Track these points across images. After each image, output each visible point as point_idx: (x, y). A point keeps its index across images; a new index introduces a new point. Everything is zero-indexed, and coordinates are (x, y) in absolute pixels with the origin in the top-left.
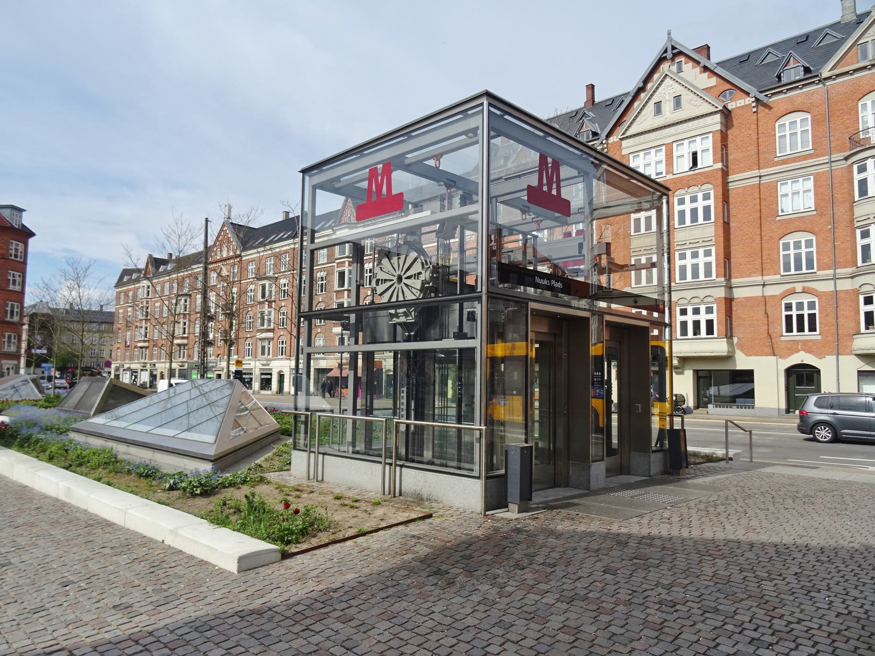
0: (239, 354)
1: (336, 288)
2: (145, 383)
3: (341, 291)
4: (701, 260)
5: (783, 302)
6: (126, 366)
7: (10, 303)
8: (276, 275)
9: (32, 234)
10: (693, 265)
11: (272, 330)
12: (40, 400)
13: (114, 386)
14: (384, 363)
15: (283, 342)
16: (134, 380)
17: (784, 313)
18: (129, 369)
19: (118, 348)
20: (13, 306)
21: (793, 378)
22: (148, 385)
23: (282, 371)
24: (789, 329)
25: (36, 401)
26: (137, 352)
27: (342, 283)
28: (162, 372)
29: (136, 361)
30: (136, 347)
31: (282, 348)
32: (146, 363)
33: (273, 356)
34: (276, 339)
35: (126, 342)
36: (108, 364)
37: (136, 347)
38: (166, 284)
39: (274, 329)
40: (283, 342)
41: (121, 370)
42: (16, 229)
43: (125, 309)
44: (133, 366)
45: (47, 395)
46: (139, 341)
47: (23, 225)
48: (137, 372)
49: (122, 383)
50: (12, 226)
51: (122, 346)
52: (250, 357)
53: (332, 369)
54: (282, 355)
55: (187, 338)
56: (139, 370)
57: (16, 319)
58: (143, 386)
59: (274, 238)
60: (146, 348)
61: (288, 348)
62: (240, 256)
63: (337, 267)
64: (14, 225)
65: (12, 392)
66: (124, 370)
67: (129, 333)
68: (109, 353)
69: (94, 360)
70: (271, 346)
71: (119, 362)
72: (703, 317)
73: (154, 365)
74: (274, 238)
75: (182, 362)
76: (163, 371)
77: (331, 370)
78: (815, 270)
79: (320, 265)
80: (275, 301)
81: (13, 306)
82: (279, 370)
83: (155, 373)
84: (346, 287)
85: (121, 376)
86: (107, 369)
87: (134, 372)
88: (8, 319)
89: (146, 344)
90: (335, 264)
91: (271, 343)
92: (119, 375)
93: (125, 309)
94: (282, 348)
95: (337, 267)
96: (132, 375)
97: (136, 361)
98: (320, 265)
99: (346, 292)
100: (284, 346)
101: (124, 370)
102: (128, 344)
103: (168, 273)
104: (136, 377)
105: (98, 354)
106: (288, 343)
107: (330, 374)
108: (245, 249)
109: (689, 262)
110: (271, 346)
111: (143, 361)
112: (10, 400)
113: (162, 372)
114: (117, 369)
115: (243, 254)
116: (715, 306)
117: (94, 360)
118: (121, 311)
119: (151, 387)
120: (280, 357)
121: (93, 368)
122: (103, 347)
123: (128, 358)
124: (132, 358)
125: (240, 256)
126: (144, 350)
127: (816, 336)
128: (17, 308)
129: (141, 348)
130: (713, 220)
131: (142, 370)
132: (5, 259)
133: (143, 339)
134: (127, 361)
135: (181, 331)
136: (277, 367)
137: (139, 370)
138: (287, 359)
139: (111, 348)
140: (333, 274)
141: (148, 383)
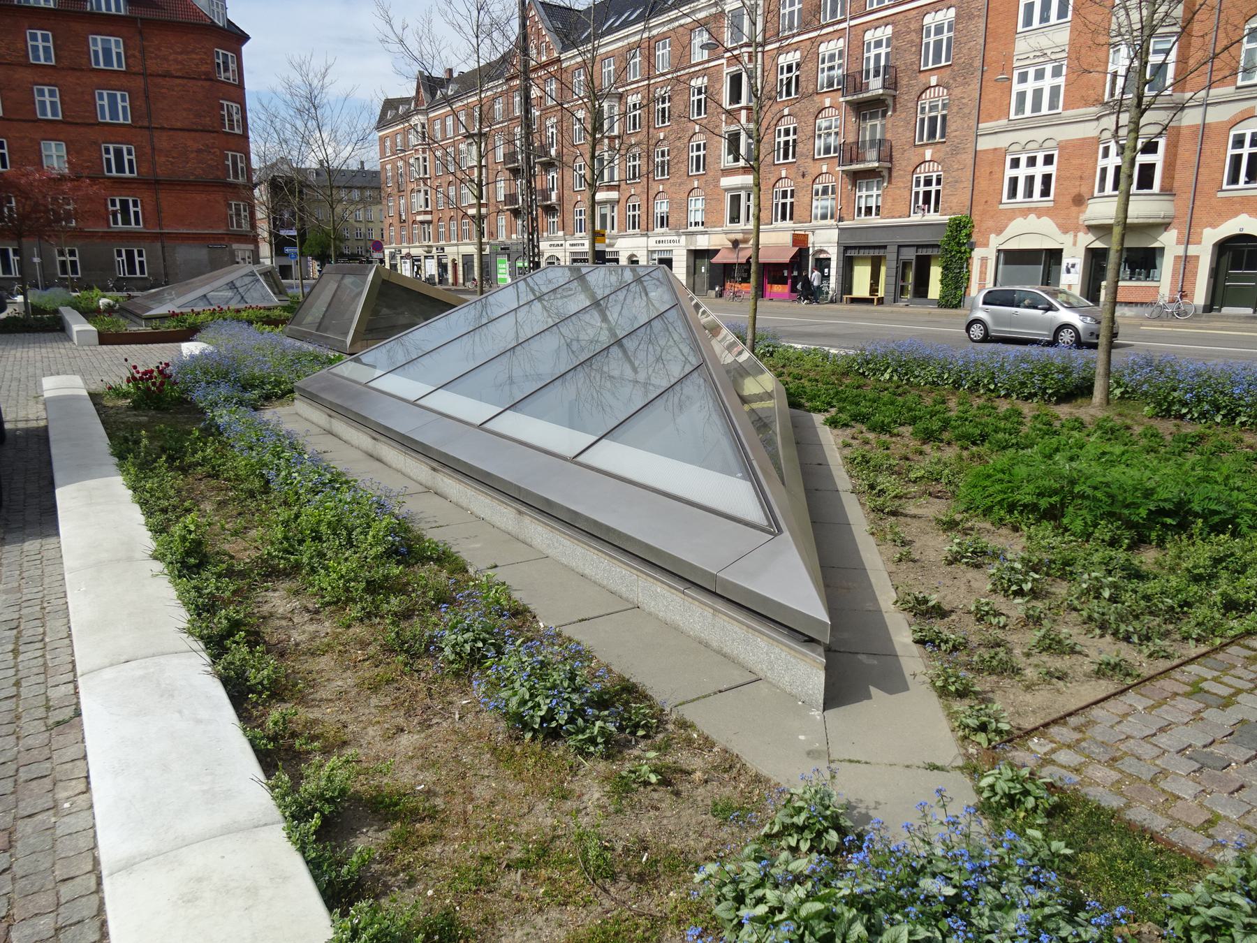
0: (566, 229)
1: (726, 104)
2: (432, 276)
3: (735, 110)
4: (1048, 82)
5: (1232, 133)
6: (404, 251)
7: (230, 153)
8: (621, 90)
9: (244, 38)
10: (1052, 88)
11: (617, 188)
12: (275, 308)
13: (385, 282)
14: (811, 239)
15: (634, 206)
16: (417, 273)
17: (1231, 152)
18: (408, 256)
19: (391, 225)
20: (234, 158)
21: (1226, 259)
22: (437, 280)
23: (633, 255)
24: (1013, 193)
25: (269, 309)
26: (417, 230)
27: (736, 96)
28: (454, 260)
29: (417, 244)
30: (414, 222)
31: (634, 216)
32: (431, 246)
33: (619, 231)
34: (623, 202)
35: (400, 215)
36: (378, 246)
37: (414, 222)
38: (448, 119)
39: (619, 186)
40: (634, 206)
41: (399, 258)
42: (219, 27)
43: (394, 163)
44: (414, 252)
45: (293, 297)
46: (419, 213)
47: (229, 21)
48: (419, 260)
49: (401, 275)
50: (213, 22)
51: (395, 221)
52: (637, 230)
53: (719, 250)
54: (784, 218)
55: (431, 212)
56: (422, 258)
57: (241, 180)
58: (430, 280)
59: (629, 16)
60: (429, 222)
61: (644, 217)
62: (559, 60)
63: (728, 66)
64: (216, 21)
65: (229, 294)
66: (402, 258)
67: (402, 201)
68: (380, 233)
69: (362, 244)
70: (615, 214)
71: (394, 245)
72: (1040, 170)
73: (443, 249)
74: (629, 16)
75: (428, 246)
76: (456, 258)
77: (717, 251)
78: (1060, 110)
79: (695, 65)
80: (619, 137)
81: (234, 158)
82: (630, 253)
83: (444, 261)
84: (744, 102)
85: (399, 267)
86: (376, 255)
87: (415, 260)
88: (231, 179)
89: (428, 217)
90: (724, 61)
91: (616, 209)
92: (395, 265)
93: (394, 163)
94: (634, 216)
95: (728, 66)
96: (413, 265)
97: (417, 244)
98: (695, 65)
99: (744, 113)
100: (637, 213)
101: (402, 258)
102: (404, 217)
103: (448, 101)
104: (419, 268)
105: (365, 235)
106: (644, 209)
107: (718, 259)
108: (565, 49)
109: (1030, 86)
110: (615, 214)
111: (426, 243)
112: (225, 308)
113: (454, 260)
114: (393, 256)
115: (563, 57)
116: (1056, 153)
117: (362, 244)
118: (389, 167)
119: (440, 282)
120: (631, 231)
121: (362, 256)
122: (370, 225)
123: (405, 239)
124: (410, 240)
125: (559, 60)
126: (426, 226)
127: (1048, 202)
128: (242, 162)
129: (422, 223)
130: (1069, 18)
131: (426, 257)
132: (211, 80)
133: (422, 209)
134: (405, 244)
135: (423, 202)
136: (626, 249)
137: (422, 258)
138: (642, 235)
139: (381, 225)
140: (719, 79)
141: (437, 276)
